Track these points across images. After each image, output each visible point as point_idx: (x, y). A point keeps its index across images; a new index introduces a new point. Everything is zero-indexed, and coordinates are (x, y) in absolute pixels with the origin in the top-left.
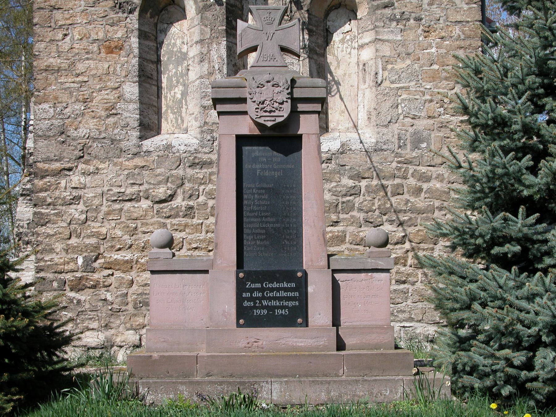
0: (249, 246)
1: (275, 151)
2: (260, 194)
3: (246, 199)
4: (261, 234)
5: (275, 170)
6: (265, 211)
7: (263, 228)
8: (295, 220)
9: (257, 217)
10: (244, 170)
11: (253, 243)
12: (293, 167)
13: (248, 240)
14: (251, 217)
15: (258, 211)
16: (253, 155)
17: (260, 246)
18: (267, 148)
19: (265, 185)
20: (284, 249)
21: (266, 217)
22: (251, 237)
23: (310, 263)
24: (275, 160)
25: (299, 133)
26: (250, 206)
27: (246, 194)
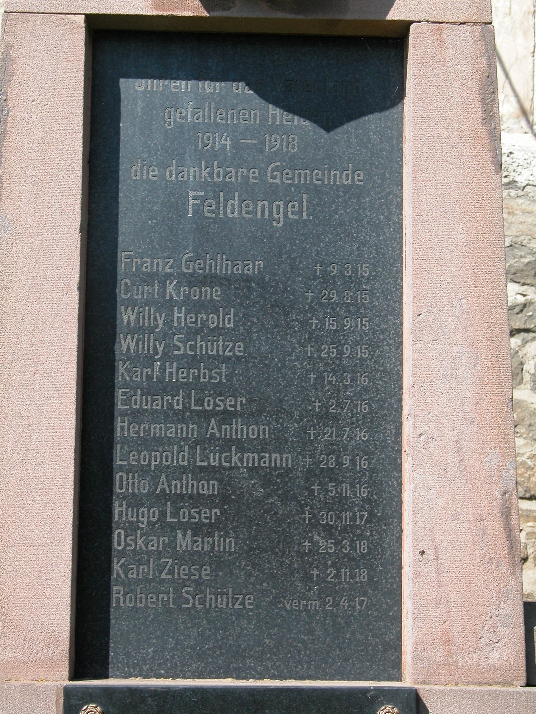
0: (139, 558)
1: (277, 103)
2: (197, 307)
3: (130, 331)
4: (196, 500)
5: (272, 194)
6: (219, 390)
7: (209, 472)
8: (362, 435)
9: (180, 417)
10: (123, 188)
11: (158, 542)
12: (359, 178)
13: (132, 528)
14: (154, 416)
15: (187, 387)
16: (172, 119)
17: (192, 558)
18: (240, 88)
19: (222, 266)
20: (307, 578)
21: (226, 417)
22: (147, 515)
23: (438, 655)
24: (273, 143)
25: (395, 14)
26: (150, 361)
27: (132, 303)
